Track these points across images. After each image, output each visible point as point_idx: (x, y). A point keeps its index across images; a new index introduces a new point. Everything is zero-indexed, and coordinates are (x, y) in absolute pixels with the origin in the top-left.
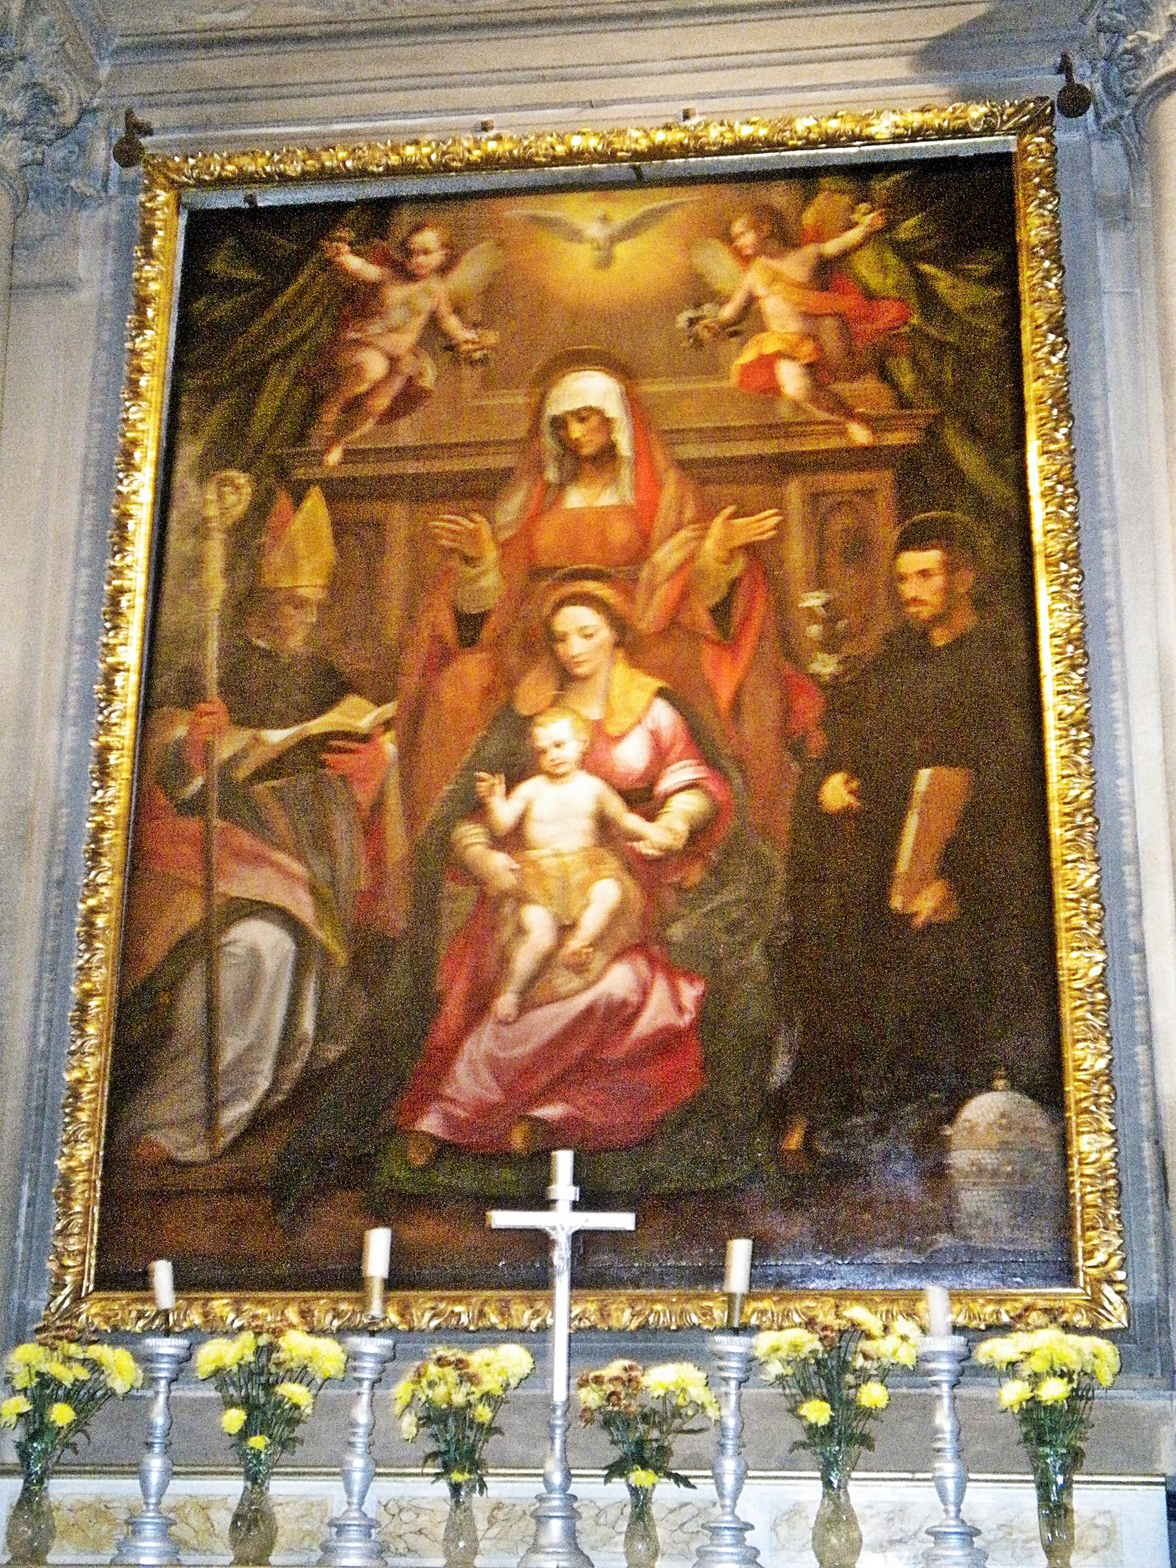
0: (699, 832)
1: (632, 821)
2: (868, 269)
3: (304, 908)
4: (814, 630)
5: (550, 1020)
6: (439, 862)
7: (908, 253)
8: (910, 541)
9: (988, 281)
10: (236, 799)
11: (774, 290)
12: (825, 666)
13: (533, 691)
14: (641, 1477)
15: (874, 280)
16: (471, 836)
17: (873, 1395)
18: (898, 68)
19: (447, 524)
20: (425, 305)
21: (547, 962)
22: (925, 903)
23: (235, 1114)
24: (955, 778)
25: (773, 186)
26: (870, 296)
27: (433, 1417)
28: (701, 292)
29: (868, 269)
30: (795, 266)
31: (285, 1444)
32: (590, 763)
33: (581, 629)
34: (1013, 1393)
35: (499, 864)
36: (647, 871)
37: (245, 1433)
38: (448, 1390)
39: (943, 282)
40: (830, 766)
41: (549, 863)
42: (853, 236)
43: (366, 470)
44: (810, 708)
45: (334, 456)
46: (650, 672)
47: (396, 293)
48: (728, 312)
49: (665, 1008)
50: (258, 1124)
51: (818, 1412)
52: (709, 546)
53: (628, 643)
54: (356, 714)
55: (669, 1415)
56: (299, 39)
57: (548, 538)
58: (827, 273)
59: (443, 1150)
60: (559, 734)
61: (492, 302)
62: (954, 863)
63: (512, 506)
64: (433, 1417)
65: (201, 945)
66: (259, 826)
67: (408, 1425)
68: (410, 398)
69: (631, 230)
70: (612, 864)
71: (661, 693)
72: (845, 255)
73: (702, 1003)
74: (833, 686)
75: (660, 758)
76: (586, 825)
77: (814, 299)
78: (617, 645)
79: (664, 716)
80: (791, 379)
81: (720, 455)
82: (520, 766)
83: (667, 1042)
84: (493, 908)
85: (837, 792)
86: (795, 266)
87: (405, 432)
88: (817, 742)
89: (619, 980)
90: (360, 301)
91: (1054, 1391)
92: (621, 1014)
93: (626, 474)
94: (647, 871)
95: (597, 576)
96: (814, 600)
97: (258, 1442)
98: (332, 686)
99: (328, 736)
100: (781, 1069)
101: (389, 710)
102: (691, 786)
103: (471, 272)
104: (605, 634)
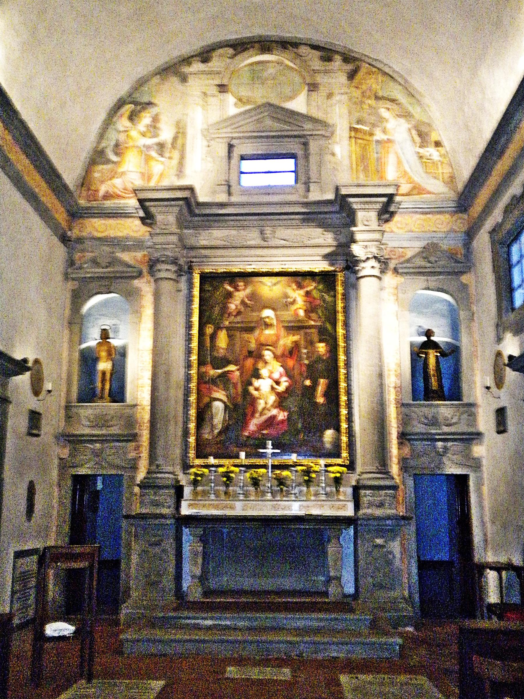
0: (287, 389)
1: (276, 386)
2: (315, 294)
3: (225, 399)
4: (305, 356)
5: (264, 418)
6: (246, 393)
7: (321, 291)
8: (320, 341)
9: (332, 296)
10: (213, 381)
11: (298, 296)
12: (306, 362)
13: (260, 365)
14: (282, 487)
15: (315, 295)
16: (251, 389)
17: (314, 475)
18: (320, 258)
19: (246, 336)
20: (241, 296)
21: (264, 409)
22: (320, 400)
23: (216, 432)
24: (327, 381)
25: (298, 277)
26: (314, 298)
27: (252, 479)
28: (286, 296)
29: (315, 294)
30: (302, 292)
31: (231, 482)
32: (270, 377)
33: (268, 355)
34: (333, 475)
35: (255, 393)
36: (278, 394)
37: (227, 481)
38: (255, 475)
39: (326, 297)
40: (307, 378)
41: (264, 393)
42: (312, 287)
43: (233, 325)
44: (304, 368)
45: (227, 323)
46: (280, 362)
47: (237, 294)
48: (292, 300)
49: (282, 416)
50: (220, 433)
51: (306, 478)
52: (288, 340)
53: (276, 357)
54: (232, 368)
55: (286, 478)
56: (217, 248)
57: (262, 339)
58: (308, 294)
59: (248, 437)
60: (264, 372)
61: (253, 296)
62: (325, 395)
63: (257, 332)
64: (252, 479)
65: (209, 406)
66: (218, 386)
67: (249, 480)
68: (239, 313)
69: (275, 284)
70: (274, 394)
71: (281, 366)
72: (311, 291)
73: (288, 415)
74: (308, 366)
75: (281, 376)
76: (270, 387)
77: (305, 298)
78: (274, 357)
79: (282, 370)
80: (302, 313)
81: (484, 227)
82: (258, 376)
83: (282, 421)
84: (253, 401)
85: (308, 383)
86: (302, 292)
87: (239, 319)
88: (305, 374)
89: (274, 412)
90: (229, 295)
91: (338, 475)
92: (273, 417)
93: (275, 328)
94: (278, 394)
95: (269, 346)
96: (305, 351)
97: (228, 482)
98: (228, 362)
99: (228, 371)
100: (300, 426)
101: (238, 367)
102: (285, 381)
103: (248, 291)
104: (272, 355)
